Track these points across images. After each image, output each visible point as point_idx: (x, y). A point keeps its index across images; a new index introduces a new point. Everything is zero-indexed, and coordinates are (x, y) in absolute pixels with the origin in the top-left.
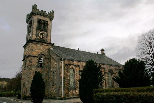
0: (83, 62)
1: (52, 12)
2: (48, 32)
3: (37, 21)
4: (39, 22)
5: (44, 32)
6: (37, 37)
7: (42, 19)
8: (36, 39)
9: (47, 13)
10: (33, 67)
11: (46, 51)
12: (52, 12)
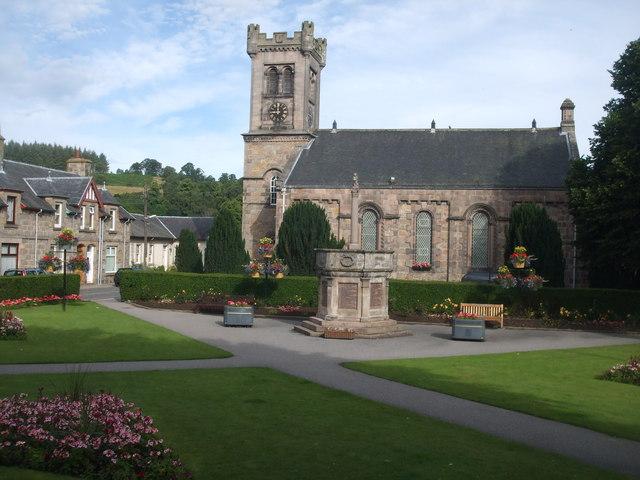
2: (296, 96)
3: (262, 74)
4: (273, 72)
6: (265, 123)
7: (275, 62)
8: (260, 128)
10: (255, 206)
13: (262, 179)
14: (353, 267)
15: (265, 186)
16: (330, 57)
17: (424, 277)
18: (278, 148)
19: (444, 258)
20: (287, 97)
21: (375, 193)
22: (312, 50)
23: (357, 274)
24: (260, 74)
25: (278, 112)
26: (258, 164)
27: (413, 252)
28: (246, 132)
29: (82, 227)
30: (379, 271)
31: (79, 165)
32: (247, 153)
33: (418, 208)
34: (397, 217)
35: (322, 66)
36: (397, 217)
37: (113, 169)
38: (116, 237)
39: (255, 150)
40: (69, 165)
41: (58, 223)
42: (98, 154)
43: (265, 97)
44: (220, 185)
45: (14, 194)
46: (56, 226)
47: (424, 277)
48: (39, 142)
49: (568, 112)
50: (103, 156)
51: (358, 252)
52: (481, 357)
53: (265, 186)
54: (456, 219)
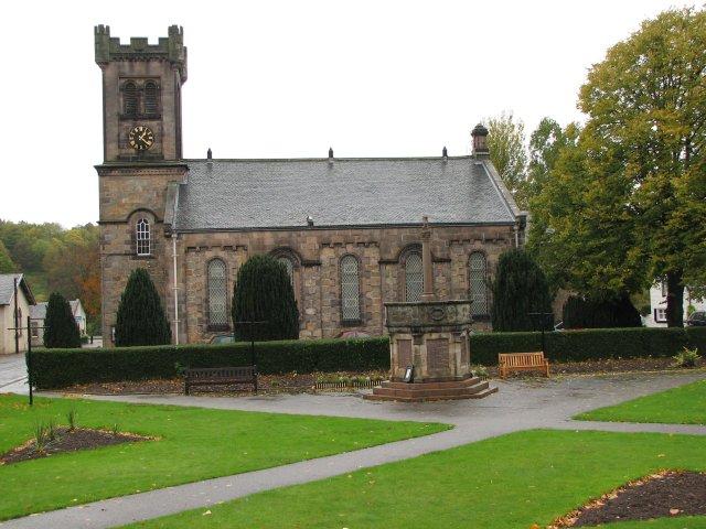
1: (176, 33)
2: (165, 118)
6: (124, 151)
8: (119, 158)
9: (150, 42)
10: (116, 258)
11: (158, 196)
12: (176, 33)
13: (126, 222)
14: (444, 321)
15: (128, 232)
18: (145, 183)
19: (376, 308)
20: (151, 118)
21: (291, 236)
22: (169, 54)
23: (448, 329)
25: (141, 138)
27: (339, 304)
28: (100, 162)
32: (102, 189)
33: (342, 252)
34: (318, 264)
36: (318, 264)
39: (113, 186)
43: (122, 118)
44: (119, 237)
49: (482, 138)
51: (449, 303)
53: (128, 232)
54: (388, 262)
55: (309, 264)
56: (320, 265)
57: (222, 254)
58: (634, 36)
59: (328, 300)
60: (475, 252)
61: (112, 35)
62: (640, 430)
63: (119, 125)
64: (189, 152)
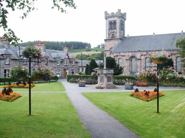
0: (129, 52)
2: (117, 29)
5: (114, 30)
16: (127, 17)
17: (5, 78)
20: (115, 29)
22: (123, 17)
24: (108, 24)
26: (108, 47)
28: (105, 39)
29: (65, 65)
30: (109, 74)
31: (66, 49)
33: (146, 57)
35: (125, 20)
37: (92, 47)
38: (74, 67)
40: (64, 49)
41: (73, 64)
42: (88, 43)
45: (47, 58)
46: (58, 65)
47: (5, 78)
48: (73, 41)
50: (89, 44)
52: (125, 92)
55: (138, 60)
56: (141, 60)
57: (121, 57)
58: (49, 41)
59: (142, 67)
60: (178, 57)
61: (108, 13)
62: (100, 92)
63: (109, 31)
64: (126, 36)
